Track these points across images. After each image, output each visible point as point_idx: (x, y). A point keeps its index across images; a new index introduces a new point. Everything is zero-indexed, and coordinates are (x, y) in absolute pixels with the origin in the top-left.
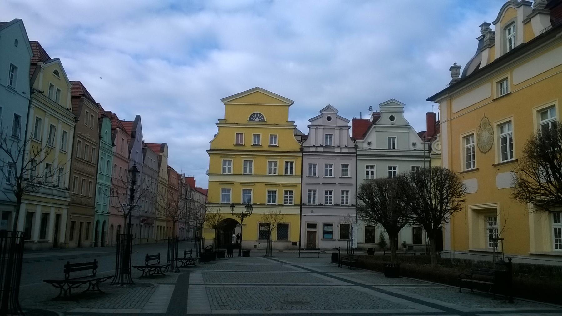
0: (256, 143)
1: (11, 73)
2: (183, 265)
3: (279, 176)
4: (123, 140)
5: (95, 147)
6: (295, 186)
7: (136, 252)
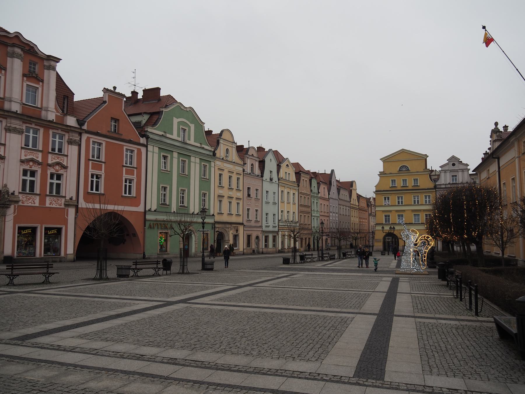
3: (421, 205)
4: (324, 188)
5: (309, 197)
7: (111, 265)
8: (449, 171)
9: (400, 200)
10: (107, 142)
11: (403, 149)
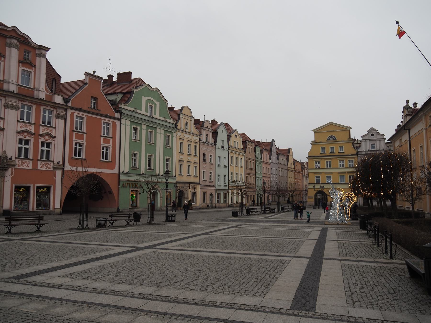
3: (346, 168)
4: (266, 154)
5: (253, 161)
8: (369, 140)
9: (329, 164)
10: (87, 116)
11: (331, 122)
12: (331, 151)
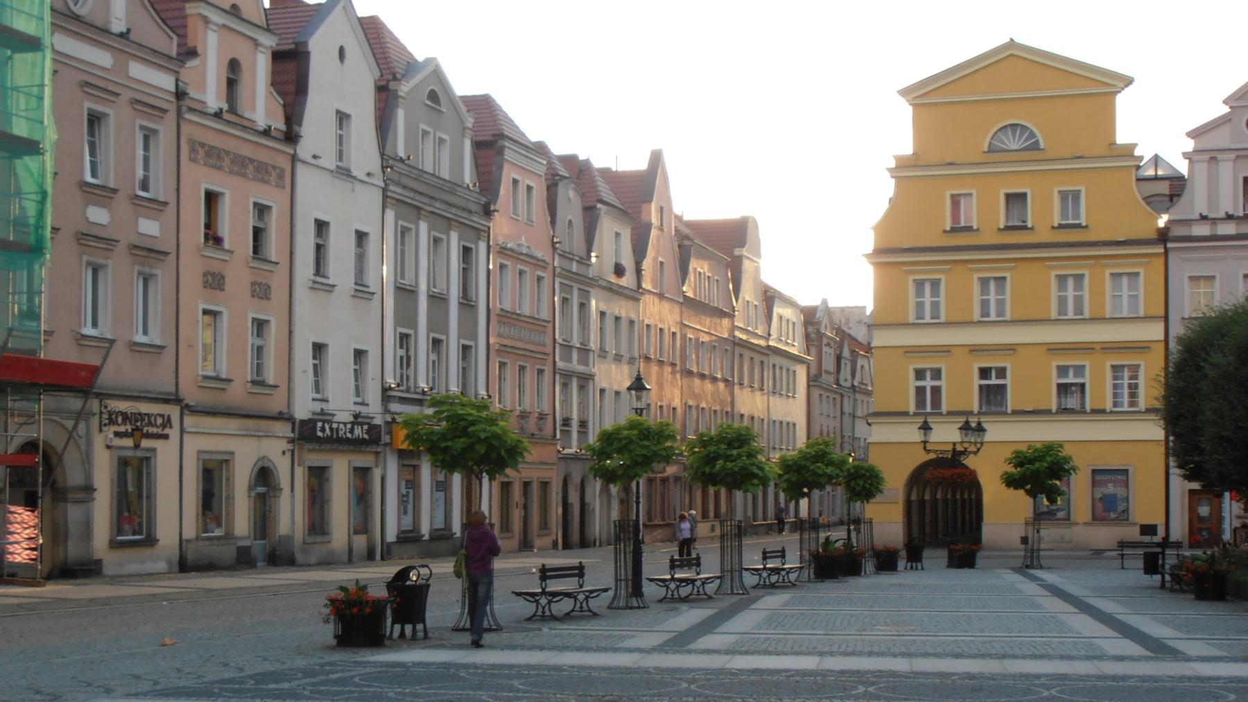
0: (1068, 220)
1: (339, 132)
2: (762, 583)
3: (1093, 319)
6: (1145, 350)
11: (1012, 43)
12: (1064, 215)
